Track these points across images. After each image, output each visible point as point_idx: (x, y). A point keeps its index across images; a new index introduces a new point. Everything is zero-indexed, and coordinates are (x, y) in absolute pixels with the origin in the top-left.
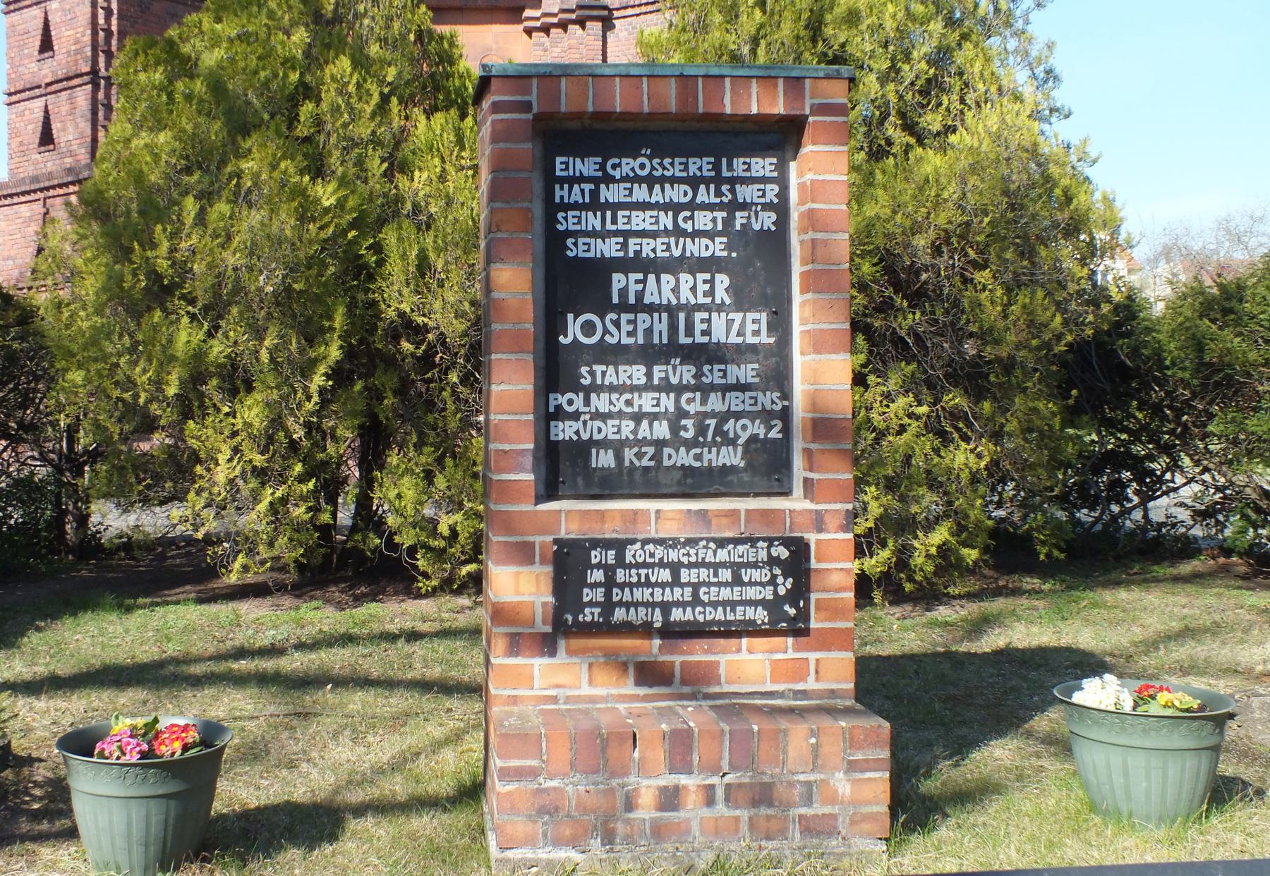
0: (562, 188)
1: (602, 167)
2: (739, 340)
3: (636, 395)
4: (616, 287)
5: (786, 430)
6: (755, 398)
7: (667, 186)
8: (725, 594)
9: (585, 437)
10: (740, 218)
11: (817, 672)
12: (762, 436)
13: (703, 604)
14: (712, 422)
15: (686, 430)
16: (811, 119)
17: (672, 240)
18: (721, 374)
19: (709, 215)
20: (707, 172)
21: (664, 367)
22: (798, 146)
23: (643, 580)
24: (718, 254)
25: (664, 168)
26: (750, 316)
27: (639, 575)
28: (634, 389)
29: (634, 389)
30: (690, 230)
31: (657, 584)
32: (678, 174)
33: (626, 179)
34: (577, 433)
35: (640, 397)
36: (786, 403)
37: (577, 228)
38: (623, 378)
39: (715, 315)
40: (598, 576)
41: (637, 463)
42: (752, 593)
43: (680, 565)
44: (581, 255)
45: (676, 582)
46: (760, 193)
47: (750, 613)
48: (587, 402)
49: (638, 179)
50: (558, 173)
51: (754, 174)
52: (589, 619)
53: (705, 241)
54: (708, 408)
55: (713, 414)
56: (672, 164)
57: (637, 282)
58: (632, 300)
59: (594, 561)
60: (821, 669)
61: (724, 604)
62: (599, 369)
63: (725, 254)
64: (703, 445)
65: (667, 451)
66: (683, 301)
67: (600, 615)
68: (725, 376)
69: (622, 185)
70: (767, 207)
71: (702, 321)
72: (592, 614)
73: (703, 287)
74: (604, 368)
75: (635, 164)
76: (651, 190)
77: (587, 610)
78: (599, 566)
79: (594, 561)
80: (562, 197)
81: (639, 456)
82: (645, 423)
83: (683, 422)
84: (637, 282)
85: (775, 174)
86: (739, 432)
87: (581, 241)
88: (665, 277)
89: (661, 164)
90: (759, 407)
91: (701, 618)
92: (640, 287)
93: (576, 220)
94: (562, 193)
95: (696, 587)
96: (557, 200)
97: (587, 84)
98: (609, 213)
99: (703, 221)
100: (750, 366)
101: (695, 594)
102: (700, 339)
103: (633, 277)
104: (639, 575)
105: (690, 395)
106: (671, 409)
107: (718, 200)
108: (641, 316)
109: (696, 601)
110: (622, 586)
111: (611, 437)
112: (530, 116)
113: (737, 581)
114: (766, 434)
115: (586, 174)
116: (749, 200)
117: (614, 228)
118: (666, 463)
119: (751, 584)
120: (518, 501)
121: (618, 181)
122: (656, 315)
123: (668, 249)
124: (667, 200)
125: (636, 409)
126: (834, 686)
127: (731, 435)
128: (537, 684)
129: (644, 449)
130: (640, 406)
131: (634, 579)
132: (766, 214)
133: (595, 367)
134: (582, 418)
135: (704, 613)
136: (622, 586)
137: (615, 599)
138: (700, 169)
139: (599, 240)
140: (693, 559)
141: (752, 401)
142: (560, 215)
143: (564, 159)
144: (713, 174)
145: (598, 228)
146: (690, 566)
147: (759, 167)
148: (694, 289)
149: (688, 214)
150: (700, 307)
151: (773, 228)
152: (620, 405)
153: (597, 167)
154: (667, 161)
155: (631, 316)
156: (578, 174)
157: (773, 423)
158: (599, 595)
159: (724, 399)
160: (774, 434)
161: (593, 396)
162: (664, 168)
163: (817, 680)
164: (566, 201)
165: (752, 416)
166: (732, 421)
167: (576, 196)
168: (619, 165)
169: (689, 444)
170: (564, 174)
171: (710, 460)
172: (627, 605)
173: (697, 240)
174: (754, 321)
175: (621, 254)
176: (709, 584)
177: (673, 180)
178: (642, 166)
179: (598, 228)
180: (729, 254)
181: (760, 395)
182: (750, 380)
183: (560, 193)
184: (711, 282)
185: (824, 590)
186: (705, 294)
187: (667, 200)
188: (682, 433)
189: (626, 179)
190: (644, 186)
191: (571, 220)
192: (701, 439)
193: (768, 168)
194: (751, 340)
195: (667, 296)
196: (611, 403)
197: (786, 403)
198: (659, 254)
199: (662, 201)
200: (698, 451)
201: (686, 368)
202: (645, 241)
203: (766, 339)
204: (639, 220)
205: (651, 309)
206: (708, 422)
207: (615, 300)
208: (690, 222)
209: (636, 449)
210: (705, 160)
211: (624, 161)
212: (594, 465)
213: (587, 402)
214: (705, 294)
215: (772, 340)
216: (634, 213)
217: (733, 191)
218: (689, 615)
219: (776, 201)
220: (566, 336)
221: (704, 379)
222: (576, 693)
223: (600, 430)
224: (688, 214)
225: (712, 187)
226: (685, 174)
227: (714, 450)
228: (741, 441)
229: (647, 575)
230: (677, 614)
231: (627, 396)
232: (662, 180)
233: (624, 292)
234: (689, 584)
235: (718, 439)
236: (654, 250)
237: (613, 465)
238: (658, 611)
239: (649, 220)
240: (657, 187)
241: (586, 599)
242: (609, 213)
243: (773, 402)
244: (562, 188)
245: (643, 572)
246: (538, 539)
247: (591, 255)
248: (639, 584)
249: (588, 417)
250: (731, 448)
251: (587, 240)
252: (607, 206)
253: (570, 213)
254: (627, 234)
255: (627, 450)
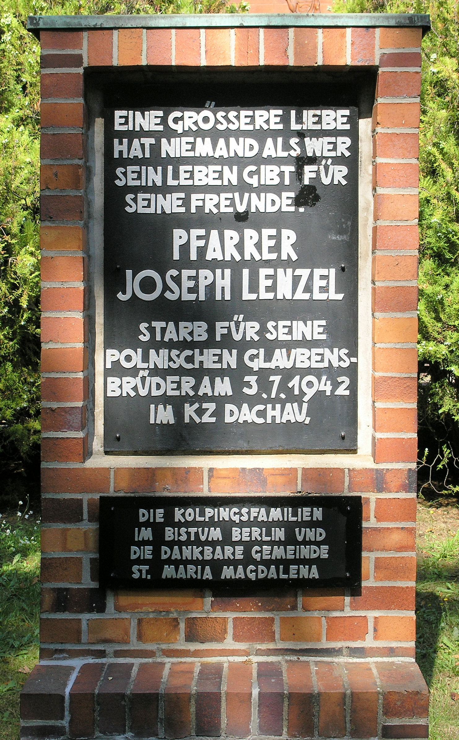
0: (121, 143)
1: (164, 120)
2: (307, 296)
3: (197, 351)
4: (177, 243)
5: (353, 387)
6: (322, 355)
7: (232, 140)
8: (278, 552)
9: (143, 392)
10: (309, 172)
11: (375, 630)
12: (328, 393)
13: (256, 563)
14: (276, 379)
15: (250, 387)
16: (380, 70)
17: (237, 195)
18: (286, 330)
19: (276, 169)
20: (275, 125)
21: (226, 324)
22: (372, 99)
23: (193, 538)
24: (285, 209)
25: (229, 121)
26: (318, 272)
27: (188, 534)
28: (192, 345)
29: (192, 345)
30: (256, 185)
31: (208, 543)
32: (243, 127)
33: (185, 133)
34: (135, 389)
35: (201, 354)
36: (354, 360)
37: (137, 183)
38: (184, 334)
39: (280, 271)
40: (146, 534)
41: (197, 420)
42: (305, 552)
43: (232, 523)
44: (141, 211)
45: (227, 540)
46: (331, 147)
47: (304, 572)
48: (146, 358)
49: (200, 133)
50: (117, 128)
51: (325, 127)
52: (136, 576)
53: (271, 196)
54: (272, 365)
55: (277, 371)
56: (238, 117)
57: (199, 238)
58: (193, 256)
59: (142, 519)
60: (379, 628)
61: (277, 562)
62: (158, 325)
63: (292, 209)
64: (265, 402)
65: (229, 407)
66: (247, 257)
67: (148, 572)
68: (290, 332)
69: (185, 139)
70: (339, 160)
71: (268, 277)
72: (140, 571)
73: (267, 243)
74: (163, 324)
75: (199, 117)
76: (214, 145)
77: (135, 568)
78: (147, 524)
79: (142, 519)
80: (121, 152)
81: (200, 412)
82: (206, 380)
83: (247, 379)
84: (199, 238)
85: (347, 127)
86: (305, 388)
87: (141, 196)
88: (228, 233)
89: (226, 118)
90: (326, 364)
91: (252, 576)
92: (202, 243)
93: (135, 176)
94: (121, 148)
95: (248, 546)
96: (116, 155)
97: (140, 37)
98: (170, 168)
99: (270, 175)
100: (316, 323)
101: (247, 552)
102: (264, 295)
103: (195, 232)
104: (188, 534)
105: (254, 352)
106: (234, 366)
107: (285, 154)
108: (203, 273)
109: (248, 560)
110: (171, 544)
111: (170, 393)
112: (81, 71)
113: (290, 540)
114: (333, 391)
115: (146, 129)
116: (318, 154)
117: (175, 183)
118: (228, 419)
119: (305, 543)
120: (67, 459)
121: (180, 135)
122: (218, 272)
123: (233, 204)
124: (232, 154)
125: (197, 366)
126: (394, 645)
127: (296, 392)
128: (84, 638)
129: (205, 406)
130: (201, 363)
131: (184, 538)
132: (338, 168)
133: (154, 324)
134: (141, 373)
135: (256, 571)
136: (171, 544)
137: (164, 557)
138: (267, 122)
139: (160, 196)
140: (245, 518)
141: (319, 358)
142: (119, 171)
143: (124, 113)
144: (280, 127)
145: (159, 184)
146: (242, 525)
147: (330, 119)
148: (258, 246)
149: (253, 168)
150: (267, 263)
151: (344, 182)
152: (181, 362)
153: (158, 121)
154: (232, 114)
155: (193, 273)
156: (137, 129)
157: (340, 379)
158: (147, 552)
159: (289, 356)
160: (342, 391)
161: (152, 352)
162: (229, 121)
163: (376, 638)
164: (125, 156)
165: (318, 373)
166: (297, 378)
167: (136, 152)
168: (182, 118)
169: (252, 401)
170: (124, 128)
171: (274, 417)
172: (177, 563)
173: (263, 195)
174: (322, 277)
175: (183, 210)
176: (261, 543)
177: (239, 134)
178: (206, 120)
179: (159, 184)
180: (297, 210)
181: (327, 351)
182: (316, 337)
183: (118, 148)
184: (278, 238)
185: (384, 549)
186: (271, 250)
187: (232, 154)
188: (246, 390)
189: (185, 133)
190: (208, 140)
191: (130, 176)
192: (265, 396)
193: (341, 120)
194: (318, 296)
195: (231, 252)
196: (170, 359)
197: (354, 360)
198: (223, 210)
199: (226, 156)
200: (261, 407)
201: (249, 324)
202: (208, 196)
203: (335, 296)
204: (202, 176)
205: (214, 265)
206: (272, 378)
207: (176, 256)
208: (256, 177)
209: (196, 406)
210: (273, 112)
211: (187, 114)
212: (152, 421)
213: (146, 358)
214: (271, 250)
215: (340, 297)
216: (197, 168)
217: (302, 145)
218: (240, 574)
219: (347, 154)
220: (124, 293)
221: (268, 336)
222: (125, 648)
223: (158, 386)
224: (253, 168)
225: (280, 140)
226: (251, 127)
227: (278, 406)
228: (306, 399)
229: (197, 534)
230: (227, 573)
231: (188, 352)
232: (227, 134)
233: (185, 248)
234: (240, 543)
235: (283, 396)
236: (217, 206)
237: (172, 421)
238: (208, 568)
239: (212, 175)
240: (221, 142)
241: (133, 557)
242: (170, 168)
243: (340, 359)
244: (121, 143)
245: (193, 530)
246: (86, 497)
247: (151, 210)
248: (188, 543)
249: (146, 373)
250: (295, 405)
251: (147, 196)
252: (170, 160)
253: (130, 168)
254: (190, 190)
255: (187, 405)
